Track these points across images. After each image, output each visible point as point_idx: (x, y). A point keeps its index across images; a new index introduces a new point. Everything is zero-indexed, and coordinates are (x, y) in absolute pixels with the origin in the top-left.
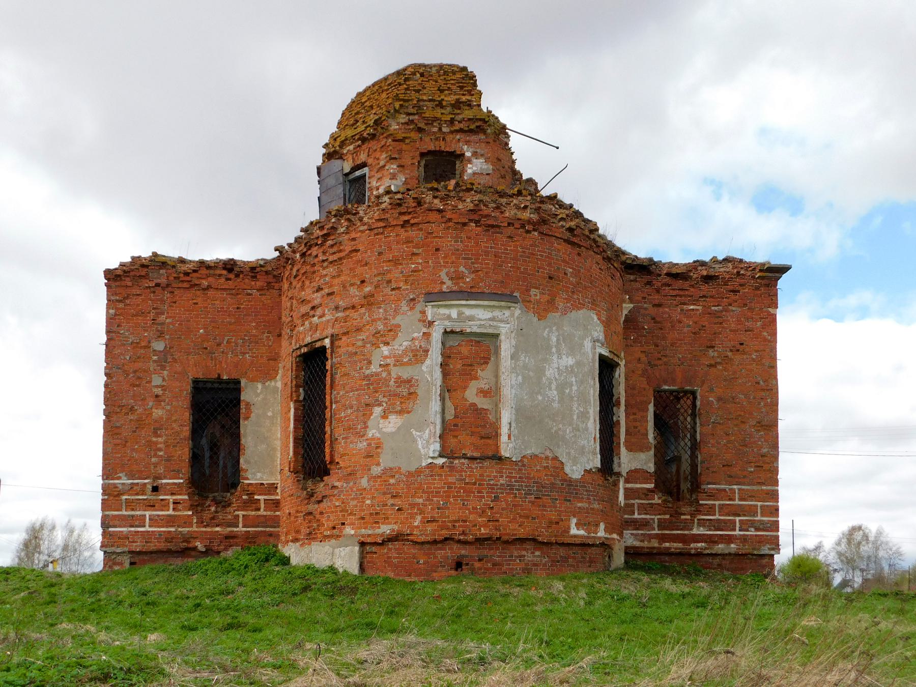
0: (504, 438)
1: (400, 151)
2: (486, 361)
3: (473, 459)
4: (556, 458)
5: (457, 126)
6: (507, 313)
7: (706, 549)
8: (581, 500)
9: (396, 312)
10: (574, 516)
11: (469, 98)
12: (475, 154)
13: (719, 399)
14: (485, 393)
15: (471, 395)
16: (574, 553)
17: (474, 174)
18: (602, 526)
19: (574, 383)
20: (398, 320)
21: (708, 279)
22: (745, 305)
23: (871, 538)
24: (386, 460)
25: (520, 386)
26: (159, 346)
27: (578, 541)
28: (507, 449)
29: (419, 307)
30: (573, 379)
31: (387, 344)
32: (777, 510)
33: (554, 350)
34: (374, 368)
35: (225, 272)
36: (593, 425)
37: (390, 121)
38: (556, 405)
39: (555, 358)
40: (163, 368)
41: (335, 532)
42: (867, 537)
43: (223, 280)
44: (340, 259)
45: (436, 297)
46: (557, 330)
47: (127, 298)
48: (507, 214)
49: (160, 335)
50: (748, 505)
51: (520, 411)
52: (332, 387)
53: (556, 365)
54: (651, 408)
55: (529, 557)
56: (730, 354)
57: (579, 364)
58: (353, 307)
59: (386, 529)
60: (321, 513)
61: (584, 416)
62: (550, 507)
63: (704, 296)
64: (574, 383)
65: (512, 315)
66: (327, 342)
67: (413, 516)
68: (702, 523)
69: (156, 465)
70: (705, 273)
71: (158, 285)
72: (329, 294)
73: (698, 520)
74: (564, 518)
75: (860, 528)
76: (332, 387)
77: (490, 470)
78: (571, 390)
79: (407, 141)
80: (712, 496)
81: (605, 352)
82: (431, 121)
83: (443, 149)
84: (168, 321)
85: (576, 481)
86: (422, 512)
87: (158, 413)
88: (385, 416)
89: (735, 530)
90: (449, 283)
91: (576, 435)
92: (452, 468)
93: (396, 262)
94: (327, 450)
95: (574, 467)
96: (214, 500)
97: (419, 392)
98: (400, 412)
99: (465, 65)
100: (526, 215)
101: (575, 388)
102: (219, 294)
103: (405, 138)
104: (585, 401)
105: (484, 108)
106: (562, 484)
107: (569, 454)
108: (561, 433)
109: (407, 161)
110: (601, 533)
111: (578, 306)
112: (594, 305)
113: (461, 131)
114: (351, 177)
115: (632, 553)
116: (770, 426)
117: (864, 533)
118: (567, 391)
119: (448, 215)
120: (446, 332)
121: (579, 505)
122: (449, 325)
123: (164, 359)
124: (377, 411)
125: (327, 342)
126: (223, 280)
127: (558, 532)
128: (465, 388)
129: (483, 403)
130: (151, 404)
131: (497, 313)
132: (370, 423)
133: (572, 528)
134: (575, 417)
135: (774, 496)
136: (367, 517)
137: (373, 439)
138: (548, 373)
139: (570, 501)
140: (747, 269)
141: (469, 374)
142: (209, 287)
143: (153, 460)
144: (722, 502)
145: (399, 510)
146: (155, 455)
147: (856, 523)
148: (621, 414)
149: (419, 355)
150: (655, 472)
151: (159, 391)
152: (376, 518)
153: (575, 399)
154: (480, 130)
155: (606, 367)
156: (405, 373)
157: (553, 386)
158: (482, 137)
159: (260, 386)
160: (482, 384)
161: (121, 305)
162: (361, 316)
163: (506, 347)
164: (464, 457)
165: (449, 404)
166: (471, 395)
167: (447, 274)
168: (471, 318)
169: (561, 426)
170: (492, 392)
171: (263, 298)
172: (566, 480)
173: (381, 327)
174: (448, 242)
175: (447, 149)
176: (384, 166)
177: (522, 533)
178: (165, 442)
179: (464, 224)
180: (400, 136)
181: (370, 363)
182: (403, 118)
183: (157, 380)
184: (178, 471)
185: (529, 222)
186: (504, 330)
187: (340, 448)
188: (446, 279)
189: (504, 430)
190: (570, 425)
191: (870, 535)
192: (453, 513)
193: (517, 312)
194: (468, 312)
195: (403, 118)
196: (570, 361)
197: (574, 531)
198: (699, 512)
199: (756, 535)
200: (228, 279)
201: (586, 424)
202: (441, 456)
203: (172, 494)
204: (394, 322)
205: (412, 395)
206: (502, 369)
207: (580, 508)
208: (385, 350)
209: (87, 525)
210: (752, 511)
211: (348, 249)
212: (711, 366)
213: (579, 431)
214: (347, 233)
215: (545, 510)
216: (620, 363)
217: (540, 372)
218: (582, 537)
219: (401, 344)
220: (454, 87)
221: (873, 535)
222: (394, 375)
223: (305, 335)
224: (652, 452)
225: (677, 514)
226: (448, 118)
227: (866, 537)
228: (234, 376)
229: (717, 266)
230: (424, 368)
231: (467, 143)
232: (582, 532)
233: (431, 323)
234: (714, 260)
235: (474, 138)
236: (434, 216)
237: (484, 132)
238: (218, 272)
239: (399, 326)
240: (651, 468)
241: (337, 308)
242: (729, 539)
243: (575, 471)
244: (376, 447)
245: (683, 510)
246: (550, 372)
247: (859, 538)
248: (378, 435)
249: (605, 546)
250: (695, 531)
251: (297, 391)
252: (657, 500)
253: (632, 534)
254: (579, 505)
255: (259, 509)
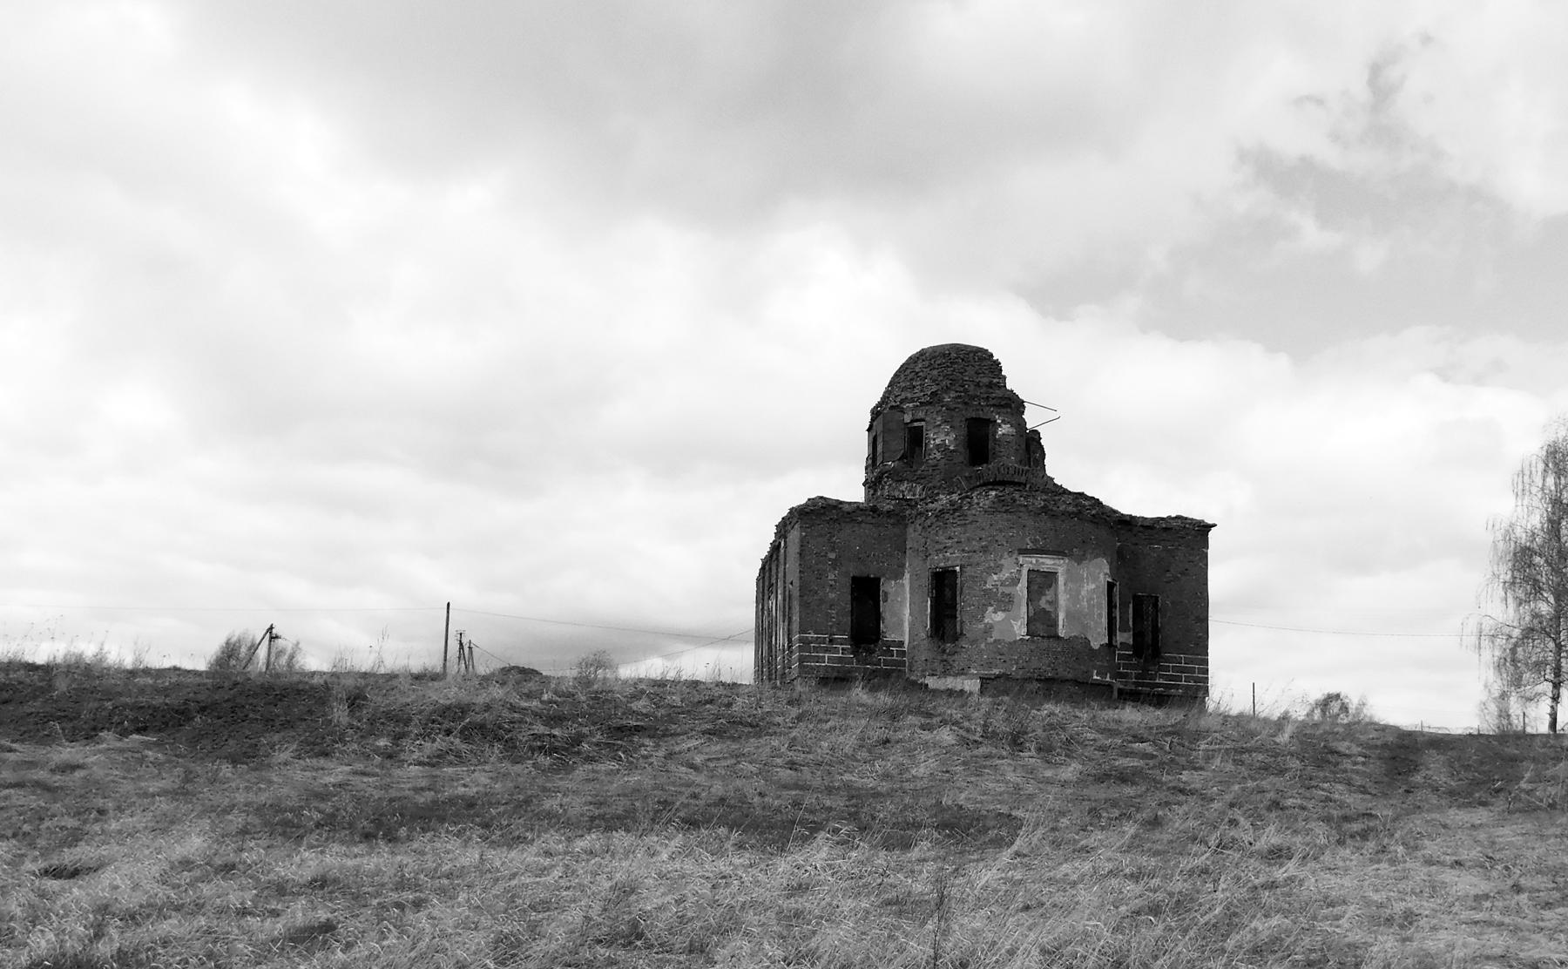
0: (1060, 627)
1: (952, 417)
2: (1050, 586)
3: (1043, 637)
4: (1086, 638)
5: (992, 402)
6: (1062, 561)
9: (1001, 557)
11: (997, 380)
12: (1003, 421)
13: (1172, 603)
14: (1050, 603)
15: (1043, 603)
17: (1003, 434)
18: (1108, 675)
20: (1003, 561)
21: (1166, 529)
22: (1189, 546)
23: (1352, 711)
24: (996, 635)
25: (1068, 600)
26: (832, 556)
28: (1062, 632)
29: (1015, 556)
31: (996, 574)
32: (1208, 670)
34: (988, 586)
35: (871, 513)
36: (1104, 620)
37: (944, 395)
38: (1086, 610)
40: (835, 569)
41: (962, 672)
42: (1347, 708)
43: (870, 518)
44: (965, 524)
45: (1024, 552)
47: (813, 525)
48: (1061, 509)
49: (833, 550)
51: (1068, 615)
52: (961, 594)
54: (1131, 605)
55: (1072, 689)
56: (1179, 575)
57: (1098, 587)
58: (975, 552)
59: (997, 671)
60: (954, 661)
61: (1100, 615)
63: (1164, 540)
65: (1064, 563)
66: (958, 569)
67: (1012, 665)
68: (1162, 676)
69: (831, 627)
70: (1164, 526)
71: (831, 519)
72: (957, 542)
75: (1338, 696)
76: (961, 594)
77: (1053, 643)
79: (957, 410)
80: (1168, 660)
81: (1110, 580)
82: (973, 398)
83: (982, 416)
84: (838, 541)
86: (1017, 664)
87: (832, 596)
88: (995, 612)
89: (1181, 681)
90: (1031, 544)
92: (1033, 642)
93: (1001, 531)
94: (958, 627)
96: (864, 648)
97: (1015, 600)
98: (1004, 611)
100: (1071, 509)
102: (868, 526)
103: (955, 408)
104: (1100, 607)
105: (1008, 387)
109: (957, 424)
110: (1108, 679)
111: (1096, 557)
112: (1105, 555)
113: (994, 405)
114: (909, 426)
115: (1121, 692)
116: (1204, 620)
117: (1343, 704)
119: (1030, 508)
120: (1029, 570)
122: (1031, 567)
123: (835, 564)
124: (990, 609)
125: (958, 569)
126: (870, 518)
128: (1040, 599)
129: (1048, 608)
130: (828, 590)
131: (1057, 562)
132: (986, 615)
135: (1206, 662)
136: (985, 665)
137: (988, 623)
140: (1190, 524)
141: (1041, 593)
142: (862, 521)
143: (830, 624)
145: (1004, 661)
146: (831, 621)
147: (1334, 691)
148: (1117, 614)
149: (1015, 581)
150: (1133, 645)
151: (833, 583)
152: (990, 665)
154: (1007, 406)
155: (1110, 586)
156: (1007, 590)
158: (1009, 410)
159: (893, 582)
160: (1048, 598)
161: (809, 530)
162: (977, 558)
163: (1061, 580)
164: (1039, 636)
165: (1030, 608)
166: (1043, 603)
167: (1030, 539)
168: (1043, 563)
170: (1054, 602)
171: (895, 530)
173: (992, 565)
174: (1030, 522)
175: (985, 417)
176: (940, 425)
177: (1070, 676)
178: (837, 614)
179: (1040, 514)
180: (952, 406)
181: (986, 583)
182: (953, 394)
183: (831, 576)
184: (845, 631)
185: (1073, 513)
186: (1060, 570)
187: (967, 627)
188: (1029, 542)
189: (1061, 623)
191: (1350, 706)
192: (1035, 664)
193: (1067, 561)
194: (1041, 560)
195: (953, 394)
196: (1093, 586)
197: (1095, 677)
198: (1160, 670)
200: (873, 517)
202: (1027, 635)
203: (841, 644)
204: (999, 563)
205: (1011, 602)
206: (1060, 591)
208: (995, 577)
210: (1192, 670)
211: (970, 519)
212: (1167, 582)
214: (968, 509)
217: (1079, 593)
219: (1005, 575)
220: (987, 372)
221: (1354, 707)
222: (1000, 591)
223: (939, 561)
224: (1131, 633)
225: (1146, 670)
226: (985, 396)
227: (1344, 708)
228: (878, 576)
229: (1172, 521)
230: (1018, 588)
231: (998, 413)
233: (1021, 565)
234: (1169, 517)
235: (1005, 410)
236: (1023, 509)
237: (1011, 408)
238: (867, 513)
239: (1003, 565)
240: (1131, 642)
241: (963, 550)
243: (1095, 645)
244: (989, 629)
245: (1150, 668)
246: (1083, 593)
247: (1336, 710)
248: (990, 622)
249: (1110, 686)
250: (1157, 681)
251: (932, 592)
252: (1134, 661)
255: (893, 656)
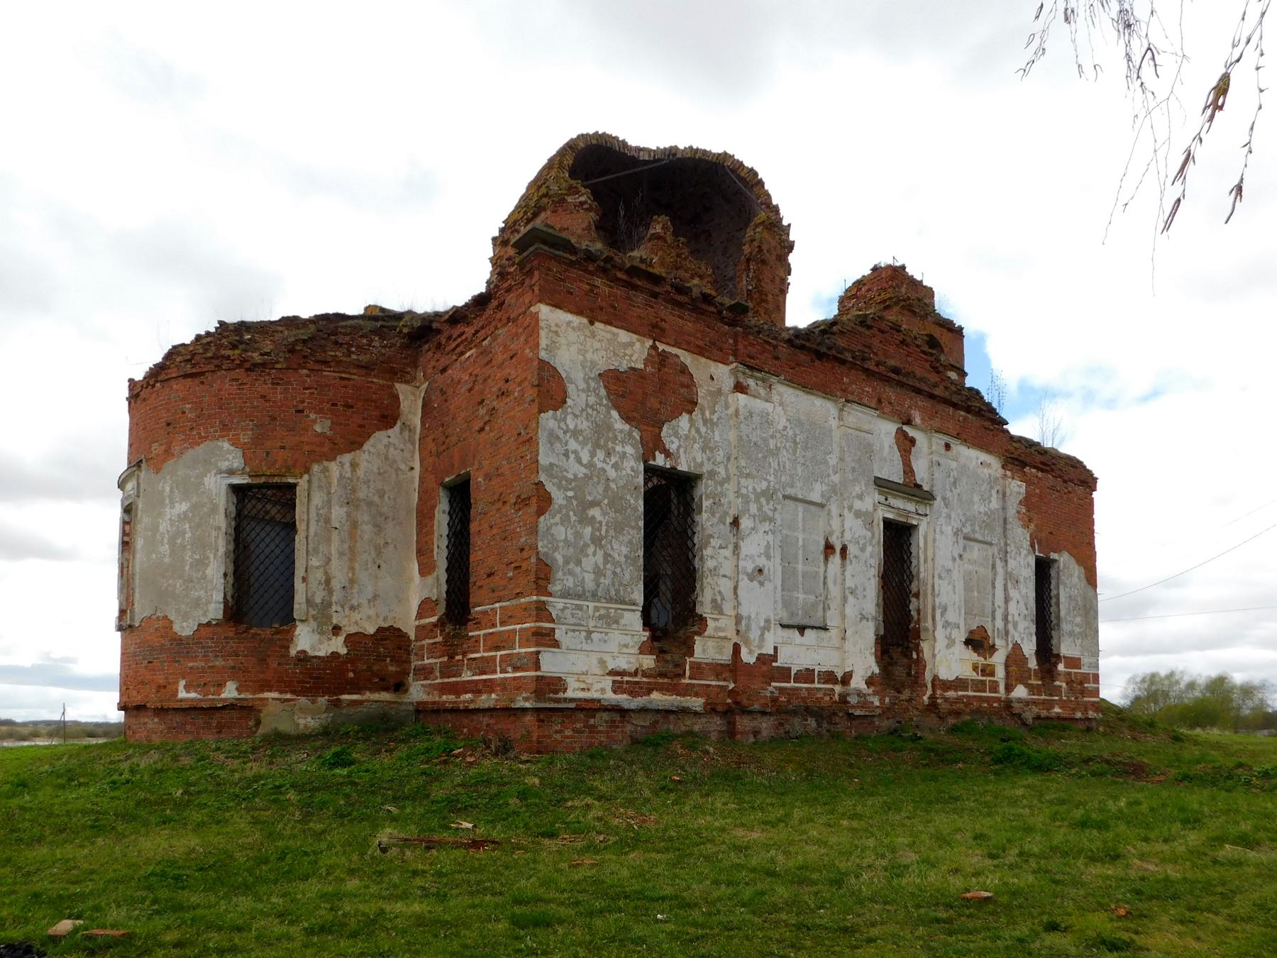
4: (165, 617)
7: (472, 701)
8: (195, 659)
10: (184, 678)
16: (193, 719)
19: (188, 529)
27: (184, 705)
30: (187, 526)
33: (167, 501)
38: (167, 560)
39: (168, 510)
46: (171, 478)
50: (507, 631)
53: (169, 517)
62: (159, 670)
64: (188, 529)
73: (468, 660)
74: (171, 681)
78: (184, 539)
85: (188, 637)
91: (187, 587)
95: (185, 624)
99: (885, 260)
101: (188, 535)
106: (171, 645)
107: (178, 610)
108: (170, 589)
118: (179, 541)
121: (191, 664)
127: (165, 696)
133: (180, 691)
134: (187, 568)
138: (161, 528)
139: (179, 661)
144: (487, 631)
153: (189, 547)
157: (166, 541)
169: (171, 581)
172: (175, 640)
190: (180, 578)
197: (182, 694)
199: (514, 678)
201: (204, 572)
207: (191, 668)
209: (945, 645)
213: (192, 581)
215: (155, 675)
216: (718, 470)
218: (192, 700)
232: (193, 695)
242: (489, 686)
246: (164, 526)
253: (422, 685)
254: (191, 664)
